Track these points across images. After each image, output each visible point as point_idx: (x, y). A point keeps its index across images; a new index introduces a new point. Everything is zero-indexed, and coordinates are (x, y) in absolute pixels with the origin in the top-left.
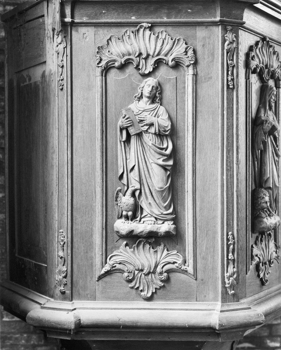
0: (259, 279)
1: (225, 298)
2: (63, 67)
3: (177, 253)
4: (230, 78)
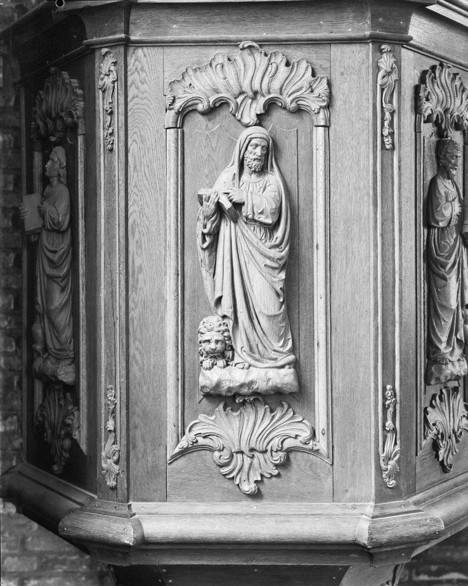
0: (438, 463)
1: (383, 495)
2: (111, 113)
3: (303, 419)
4: (386, 133)
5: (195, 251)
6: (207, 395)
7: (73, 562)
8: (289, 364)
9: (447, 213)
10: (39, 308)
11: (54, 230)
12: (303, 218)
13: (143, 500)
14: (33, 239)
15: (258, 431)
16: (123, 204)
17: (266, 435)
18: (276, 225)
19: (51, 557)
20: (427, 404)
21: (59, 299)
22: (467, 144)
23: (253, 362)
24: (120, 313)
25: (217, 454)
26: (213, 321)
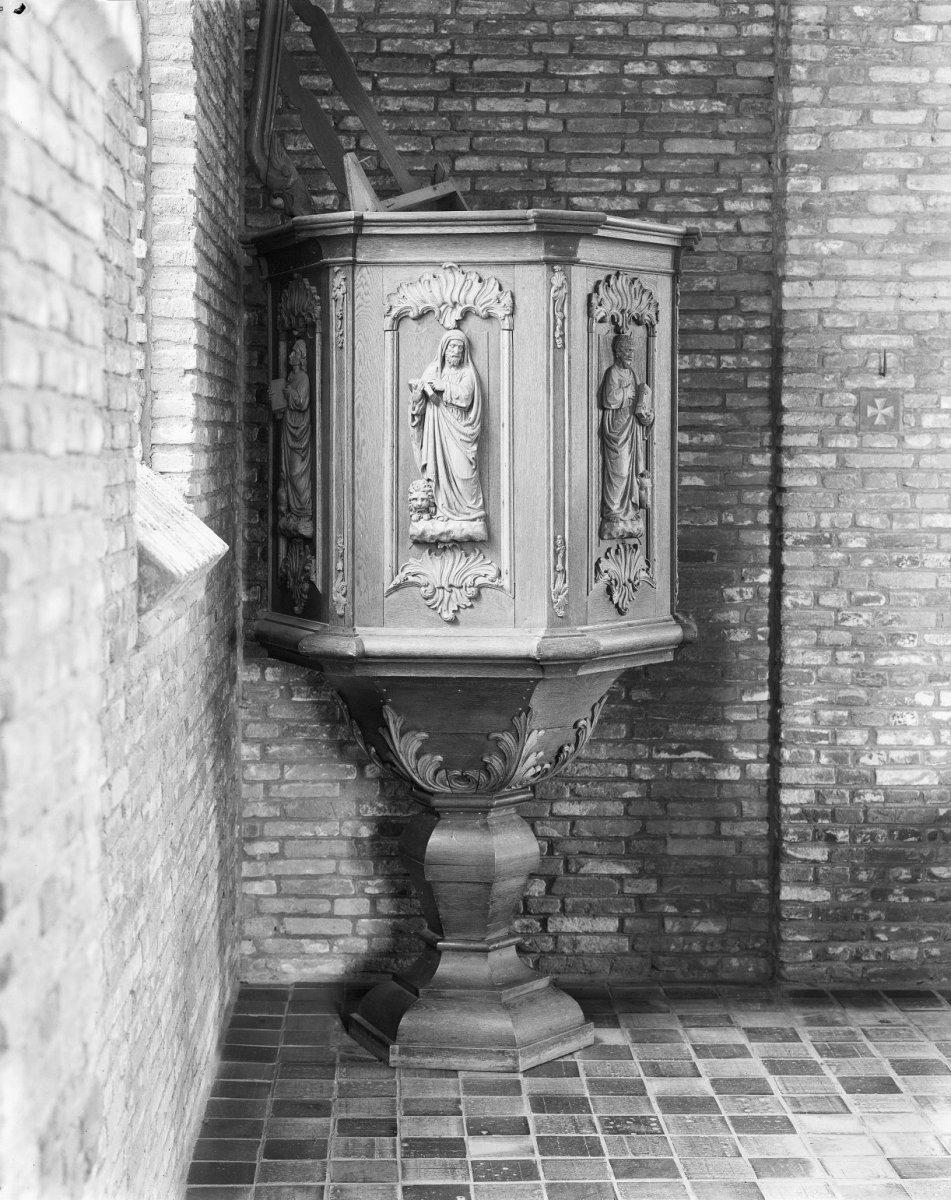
2: (342, 319)
4: (557, 335)
5: (407, 429)
6: (416, 542)
7: (314, 730)
8: (480, 518)
9: (619, 397)
10: (284, 475)
11: (295, 410)
12: (492, 403)
13: (366, 626)
14: (279, 417)
15: (455, 571)
16: (350, 390)
17: (461, 573)
18: (471, 407)
19: (293, 724)
20: (602, 555)
21: (300, 467)
22: (934, 248)
23: (451, 516)
24: (347, 477)
25: (423, 589)
26: (420, 483)
